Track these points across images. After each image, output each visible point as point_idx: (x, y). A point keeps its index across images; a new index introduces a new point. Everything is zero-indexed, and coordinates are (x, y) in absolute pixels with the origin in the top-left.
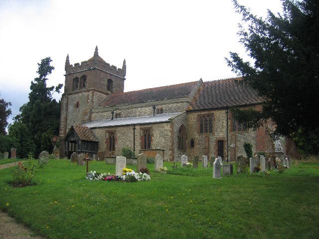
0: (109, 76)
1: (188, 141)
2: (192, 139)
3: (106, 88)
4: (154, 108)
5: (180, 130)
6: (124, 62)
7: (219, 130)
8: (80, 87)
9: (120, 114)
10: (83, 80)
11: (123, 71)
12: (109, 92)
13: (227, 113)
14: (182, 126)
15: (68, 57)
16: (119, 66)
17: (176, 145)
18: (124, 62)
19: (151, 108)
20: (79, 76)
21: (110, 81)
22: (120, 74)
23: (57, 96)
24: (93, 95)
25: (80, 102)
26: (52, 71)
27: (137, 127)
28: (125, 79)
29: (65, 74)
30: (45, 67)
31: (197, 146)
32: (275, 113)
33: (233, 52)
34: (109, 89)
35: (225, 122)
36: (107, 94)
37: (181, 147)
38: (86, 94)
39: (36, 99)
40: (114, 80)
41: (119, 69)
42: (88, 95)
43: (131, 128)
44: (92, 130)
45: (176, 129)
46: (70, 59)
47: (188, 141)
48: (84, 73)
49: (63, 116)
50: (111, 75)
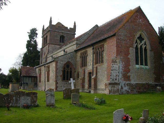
6: (75, 23)
17: (60, 79)
18: (75, 23)
36: (60, 45)
50: (63, 33)
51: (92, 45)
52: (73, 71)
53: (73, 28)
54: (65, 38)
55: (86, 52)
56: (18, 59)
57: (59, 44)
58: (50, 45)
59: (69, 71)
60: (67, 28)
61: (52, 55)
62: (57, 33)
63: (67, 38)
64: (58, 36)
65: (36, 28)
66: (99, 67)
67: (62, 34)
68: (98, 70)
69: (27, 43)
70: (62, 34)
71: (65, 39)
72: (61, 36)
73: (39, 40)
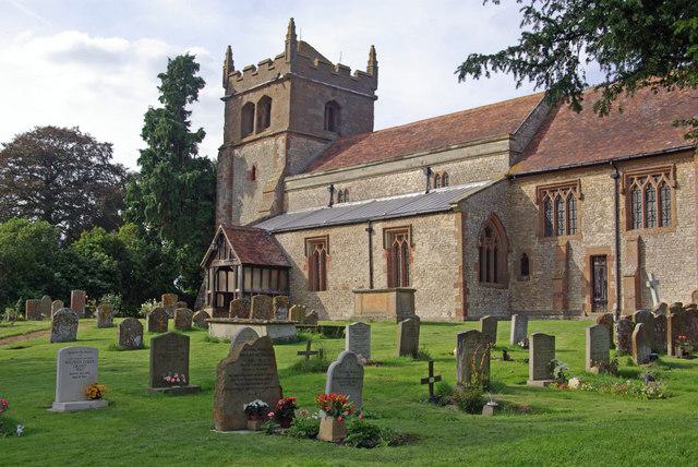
0: (329, 92)
1: (512, 262)
3: (320, 125)
4: (429, 173)
5: (488, 232)
6: (373, 53)
7: (594, 227)
8: (259, 125)
11: (369, 79)
12: (332, 135)
13: (617, 177)
14: (493, 217)
15: (230, 53)
16: (358, 64)
17: (474, 273)
18: (373, 53)
19: (420, 173)
21: (332, 108)
22: (197, 67)
23: (209, 149)
24: (288, 147)
25: (259, 168)
27: (378, 227)
28: (376, 98)
30: (181, 79)
31: (536, 273)
32: (67, 239)
35: (609, 200)
36: (326, 140)
37: (492, 276)
38: (270, 142)
39: (156, 160)
41: (359, 73)
42: (277, 147)
44: (277, 236)
45: (475, 228)
47: (512, 262)
49: (222, 202)
50: (336, 89)
51: (615, 164)
52: (501, 250)
53: (364, 69)
54: (343, 112)
55: (572, 193)
56: (163, 452)
57: (319, 135)
58: (295, 140)
59: (492, 248)
60: (347, 70)
61: (327, 179)
62: (314, 89)
63: (347, 113)
64: (319, 102)
65: (161, 76)
66: (649, 242)
67: (333, 95)
68: (648, 250)
69: (145, 146)
70: (333, 95)
71: (344, 118)
72: (330, 102)
73: (207, 117)
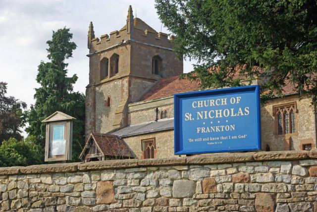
0: (154, 50)
2: (267, 145)
3: (150, 71)
8: (111, 72)
9: (166, 112)
10: (114, 62)
12: (157, 77)
20: (108, 55)
23: (278, 48)
25: (112, 99)
26: (74, 52)
29: (88, 53)
33: (33, 97)
34: (156, 73)
40: (163, 56)
42: (123, 85)
43: (262, 190)
46: (94, 29)
48: (115, 51)
50: (159, 48)
